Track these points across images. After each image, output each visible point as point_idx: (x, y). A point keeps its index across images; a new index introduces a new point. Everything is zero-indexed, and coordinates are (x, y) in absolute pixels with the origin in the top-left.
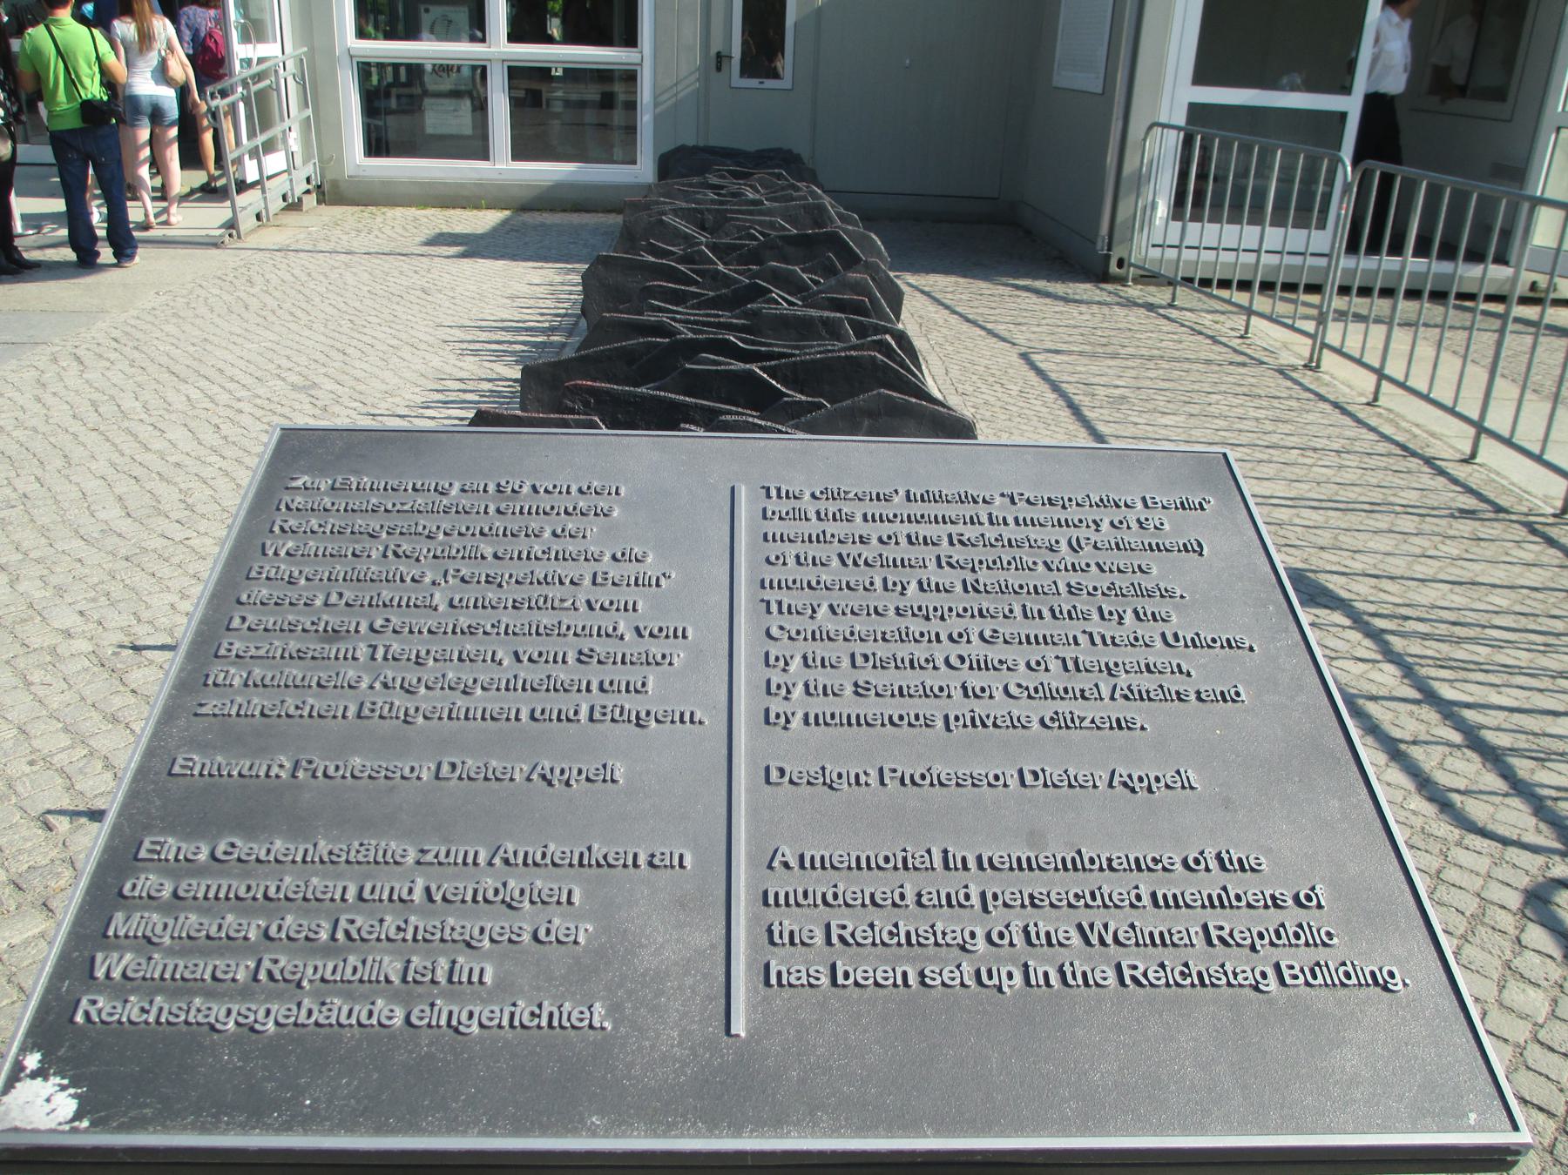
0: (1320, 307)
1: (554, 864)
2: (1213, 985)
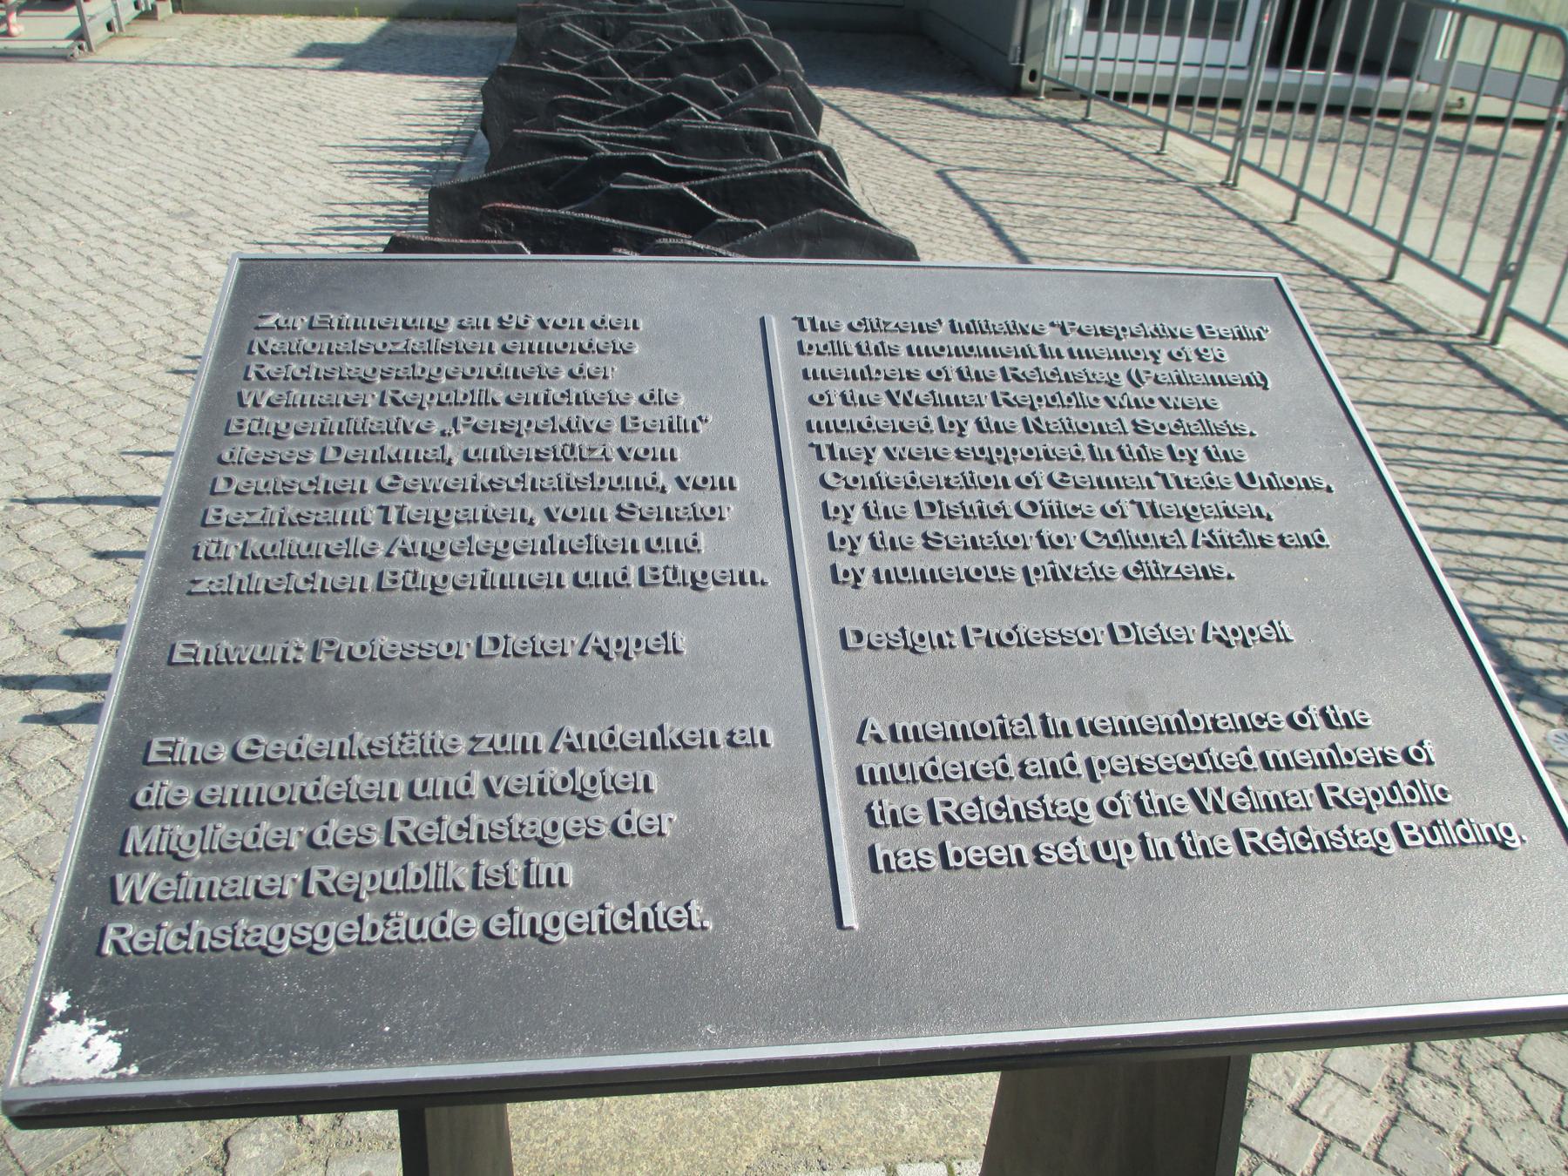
0: (1238, 123)
1: (624, 748)
2: (1334, 849)
